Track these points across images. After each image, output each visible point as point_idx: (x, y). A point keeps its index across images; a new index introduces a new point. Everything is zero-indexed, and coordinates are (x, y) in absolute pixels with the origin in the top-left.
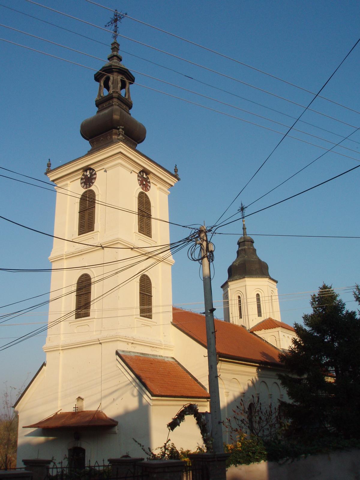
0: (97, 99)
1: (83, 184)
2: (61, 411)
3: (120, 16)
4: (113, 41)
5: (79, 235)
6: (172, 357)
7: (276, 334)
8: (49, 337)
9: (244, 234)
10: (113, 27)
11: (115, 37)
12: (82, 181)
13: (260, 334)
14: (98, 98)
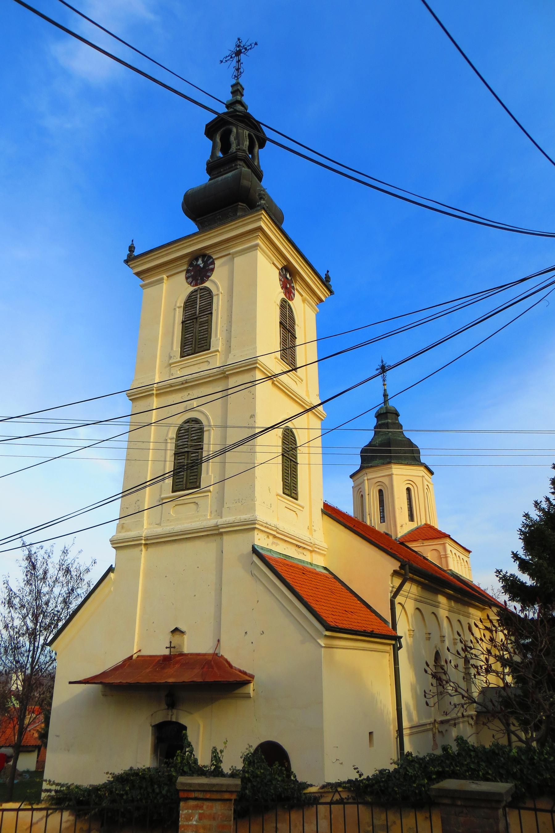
0: (210, 161)
1: (190, 280)
2: (139, 654)
3: (245, 47)
4: (234, 81)
5: (182, 356)
6: (323, 567)
7: (440, 548)
8: (123, 522)
9: (386, 402)
10: (234, 63)
11: (237, 77)
12: (189, 274)
13: (415, 546)
14: (211, 160)
